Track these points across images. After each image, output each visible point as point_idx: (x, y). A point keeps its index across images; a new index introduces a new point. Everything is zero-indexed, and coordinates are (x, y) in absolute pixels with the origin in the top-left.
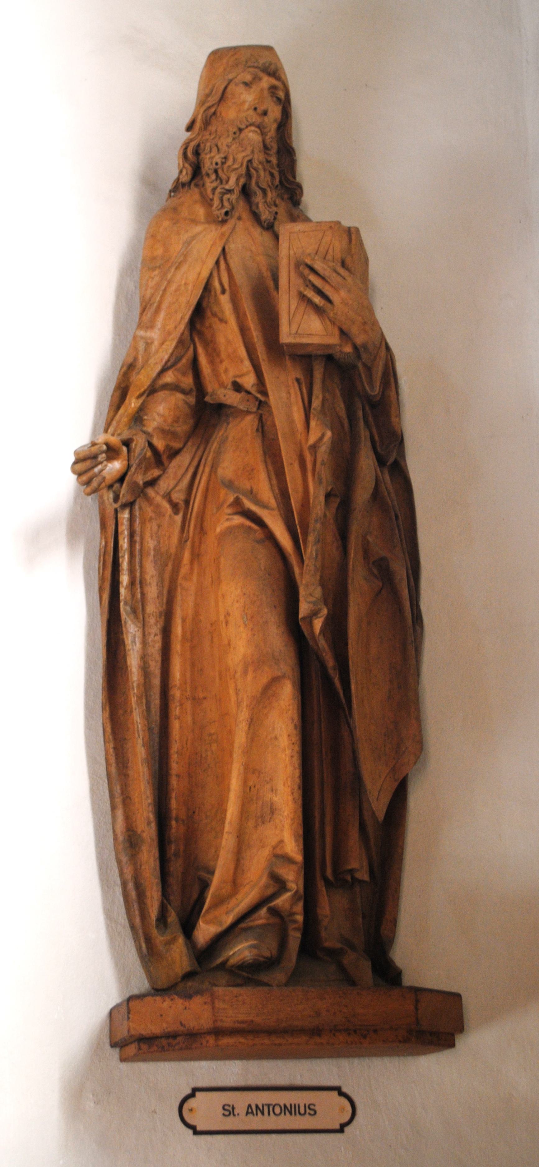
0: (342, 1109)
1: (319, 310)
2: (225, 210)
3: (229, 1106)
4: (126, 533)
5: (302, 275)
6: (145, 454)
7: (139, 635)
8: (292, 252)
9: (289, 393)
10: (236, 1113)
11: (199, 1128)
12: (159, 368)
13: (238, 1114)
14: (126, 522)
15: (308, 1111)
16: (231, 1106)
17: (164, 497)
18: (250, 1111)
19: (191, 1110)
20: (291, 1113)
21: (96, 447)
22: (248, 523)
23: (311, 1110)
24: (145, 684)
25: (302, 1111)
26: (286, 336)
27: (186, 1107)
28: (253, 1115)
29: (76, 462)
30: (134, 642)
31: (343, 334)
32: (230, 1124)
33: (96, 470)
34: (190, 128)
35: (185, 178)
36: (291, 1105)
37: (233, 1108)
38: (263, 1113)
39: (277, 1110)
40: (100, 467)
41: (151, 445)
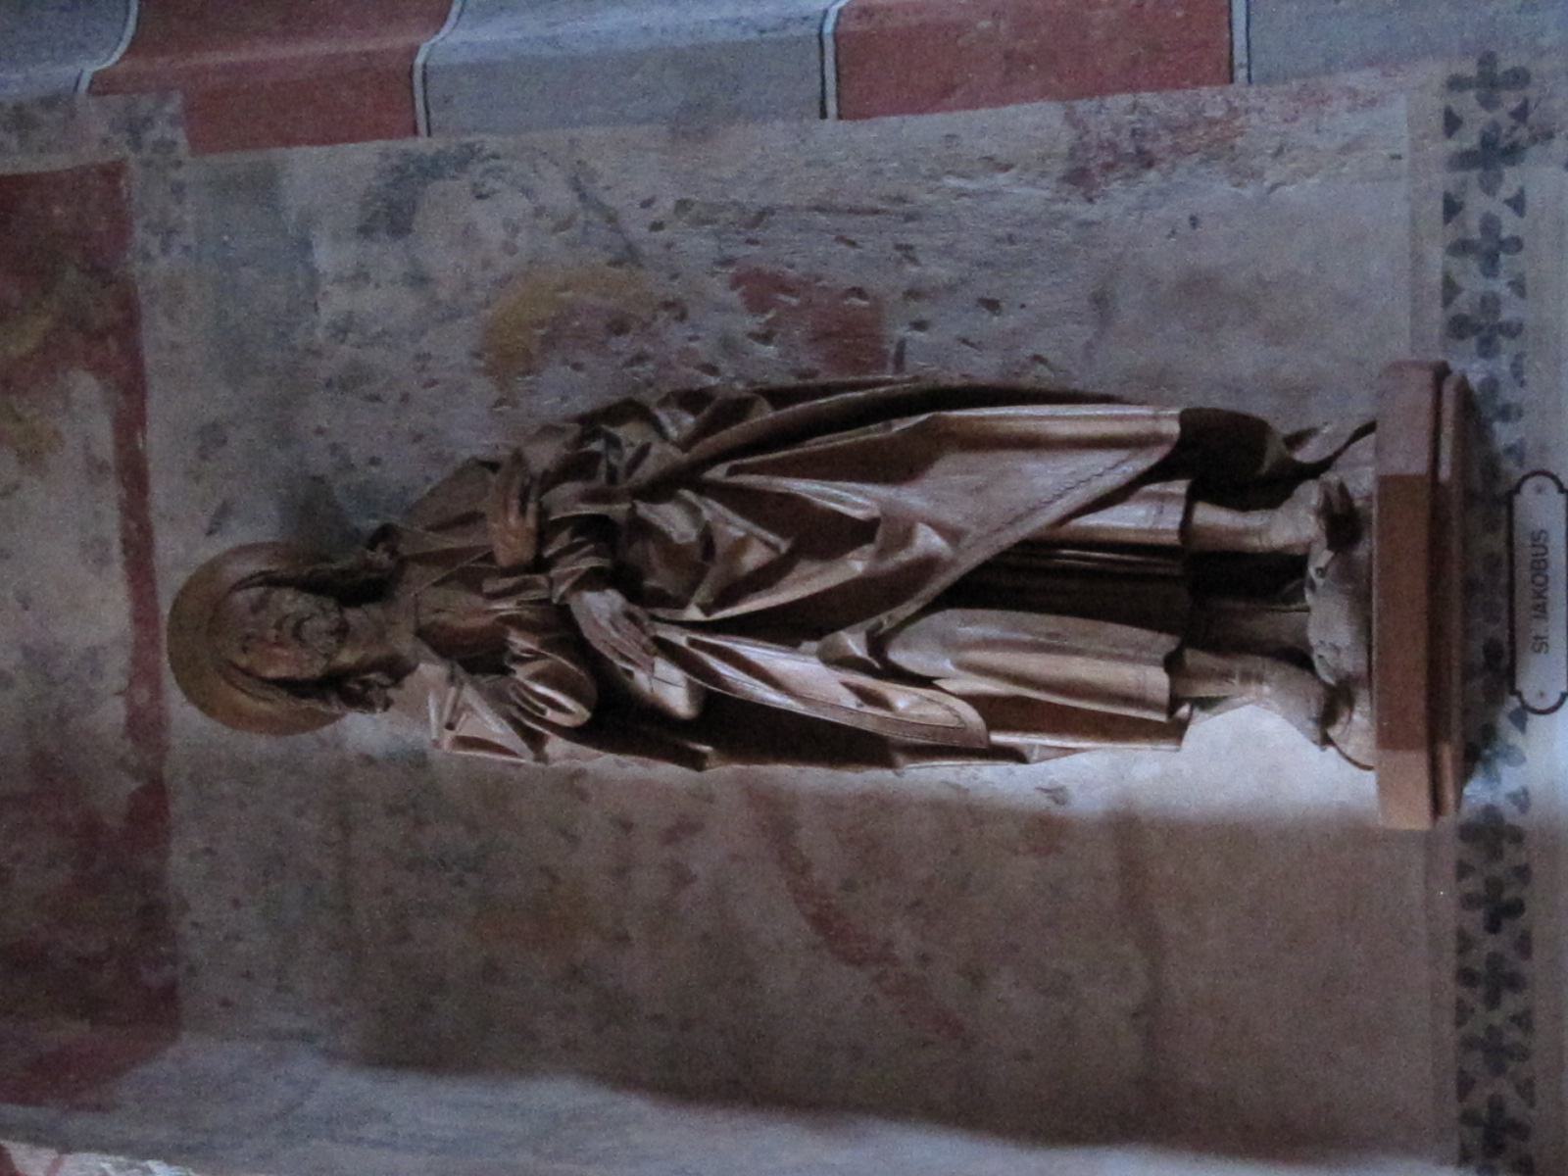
39: (1540, 579)
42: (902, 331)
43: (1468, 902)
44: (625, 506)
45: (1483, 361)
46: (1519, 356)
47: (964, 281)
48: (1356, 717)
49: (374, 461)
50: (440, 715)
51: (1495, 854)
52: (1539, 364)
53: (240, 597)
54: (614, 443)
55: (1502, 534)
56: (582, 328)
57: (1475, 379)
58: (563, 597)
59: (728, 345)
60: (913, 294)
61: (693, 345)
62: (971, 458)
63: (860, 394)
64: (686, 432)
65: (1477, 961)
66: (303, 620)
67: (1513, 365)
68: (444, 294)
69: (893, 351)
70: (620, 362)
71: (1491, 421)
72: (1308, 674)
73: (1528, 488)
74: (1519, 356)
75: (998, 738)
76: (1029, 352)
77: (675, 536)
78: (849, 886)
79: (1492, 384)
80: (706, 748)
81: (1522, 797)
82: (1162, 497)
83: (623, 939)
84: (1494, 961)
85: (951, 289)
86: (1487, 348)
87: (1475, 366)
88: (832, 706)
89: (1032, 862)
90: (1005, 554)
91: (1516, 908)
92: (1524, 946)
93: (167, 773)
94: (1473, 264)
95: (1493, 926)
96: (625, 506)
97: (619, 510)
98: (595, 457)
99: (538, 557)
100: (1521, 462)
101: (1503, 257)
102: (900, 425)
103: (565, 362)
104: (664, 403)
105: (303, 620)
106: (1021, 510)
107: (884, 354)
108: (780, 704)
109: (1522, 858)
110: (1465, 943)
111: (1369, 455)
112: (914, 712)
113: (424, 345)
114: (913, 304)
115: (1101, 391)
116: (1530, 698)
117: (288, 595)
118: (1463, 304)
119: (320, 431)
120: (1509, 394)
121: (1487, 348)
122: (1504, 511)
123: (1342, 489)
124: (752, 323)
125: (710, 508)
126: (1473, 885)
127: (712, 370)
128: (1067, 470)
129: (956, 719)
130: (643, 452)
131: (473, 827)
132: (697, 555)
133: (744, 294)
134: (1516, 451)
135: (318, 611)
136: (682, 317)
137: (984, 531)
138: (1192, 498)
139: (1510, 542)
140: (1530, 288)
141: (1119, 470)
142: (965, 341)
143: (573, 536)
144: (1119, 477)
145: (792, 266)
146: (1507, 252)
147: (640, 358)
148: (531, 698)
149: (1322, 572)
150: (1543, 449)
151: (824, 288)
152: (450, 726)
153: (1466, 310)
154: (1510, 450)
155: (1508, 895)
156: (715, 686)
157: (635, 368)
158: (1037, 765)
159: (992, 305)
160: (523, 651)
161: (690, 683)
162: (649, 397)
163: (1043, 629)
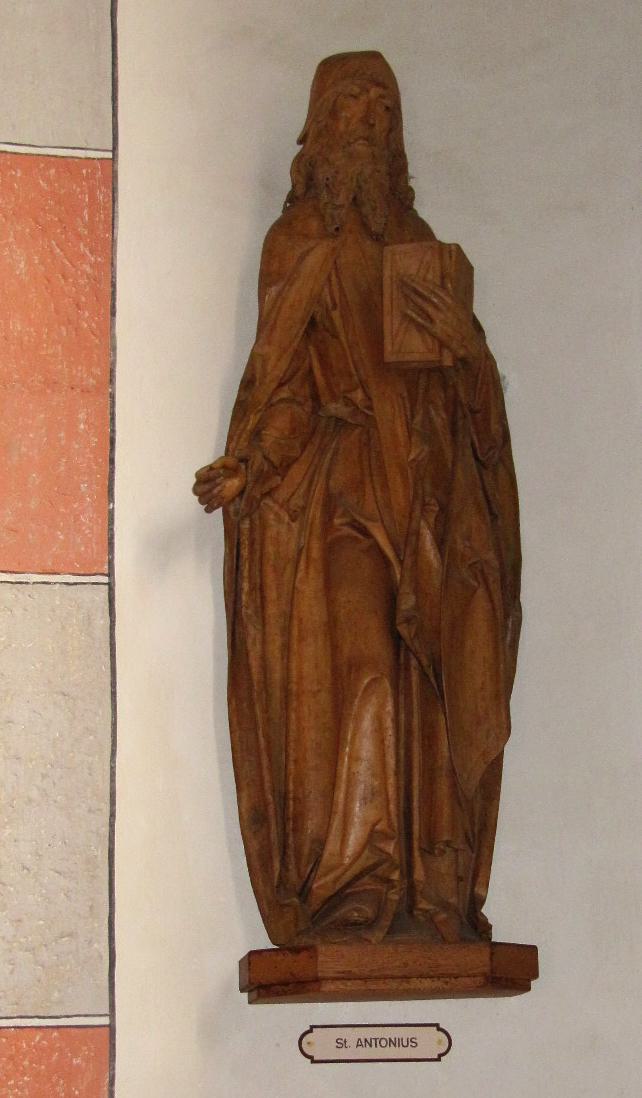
0: (440, 1042)
1: (420, 328)
2: (336, 226)
4: (247, 542)
5: (406, 297)
7: (259, 636)
8: (394, 274)
9: (393, 407)
11: (435, 1028)
12: (274, 385)
14: (246, 532)
17: (282, 506)
19: (309, 1043)
20: (395, 1045)
21: (213, 472)
22: (355, 533)
23: (412, 1042)
24: (265, 682)
25: (405, 1044)
26: (390, 356)
27: (304, 1046)
29: (196, 484)
30: (254, 644)
31: (442, 345)
32: (343, 1054)
33: (215, 491)
34: (301, 141)
35: (300, 191)
37: (345, 1042)
38: (371, 1046)
39: (383, 1043)
40: (219, 488)
41: (266, 458)
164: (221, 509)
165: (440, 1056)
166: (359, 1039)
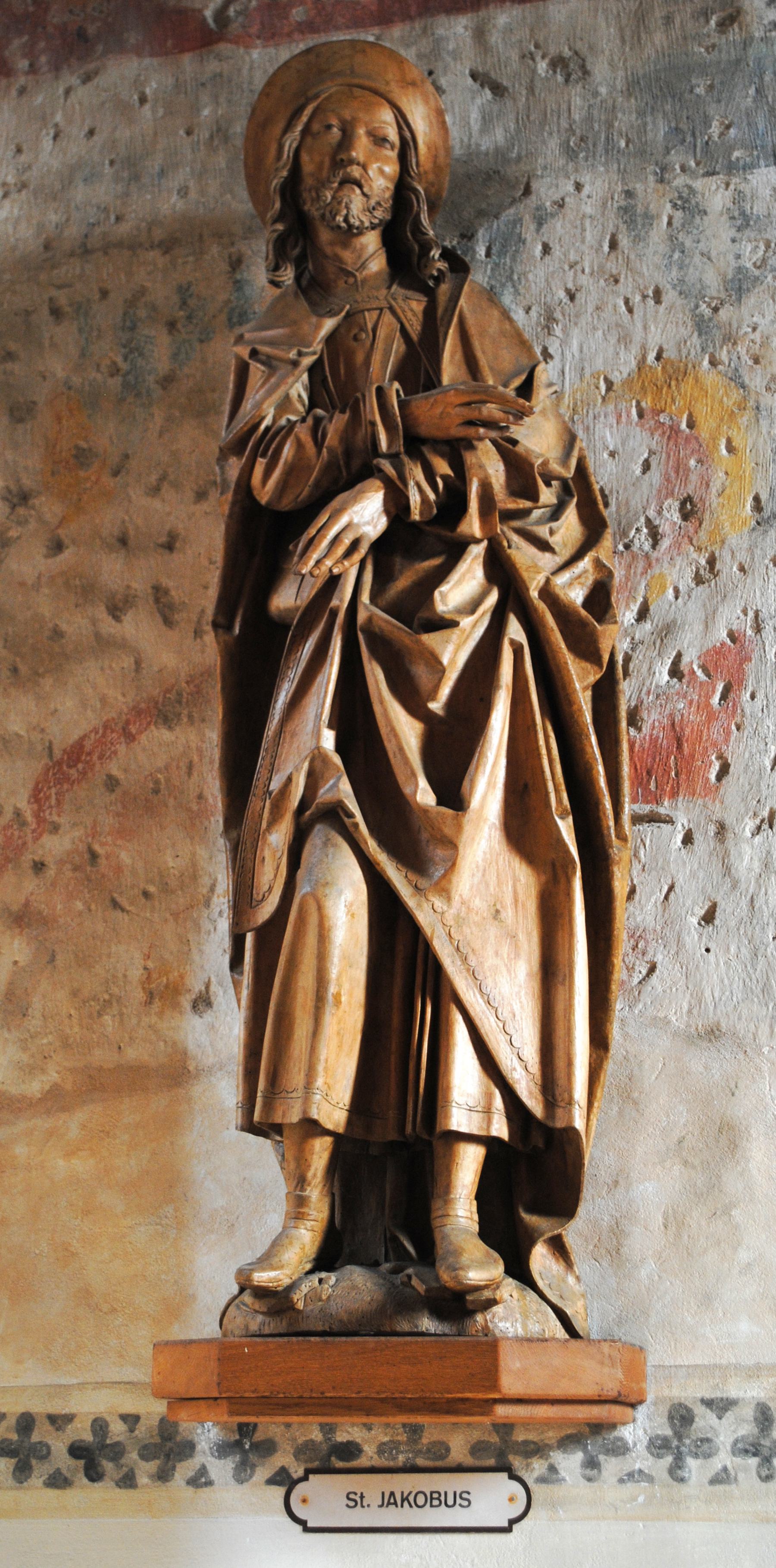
3: (356, 1494)
6: (175, 205)
10: (365, 1504)
11: (310, 1524)
13: (368, 1506)
15: (459, 1501)
16: (359, 1495)
18: (392, 1501)
28: (397, 1506)
36: (402, 1506)
37: (362, 1497)
39: (421, 1500)
42: (682, 821)
43: (100, 1426)
44: (477, 532)
45: (645, 1442)
46: (650, 1479)
47: (735, 885)
48: (260, 1318)
49: (546, 249)
50: (271, 343)
51: (146, 1454)
52: (641, 1499)
53: (387, 116)
54: (556, 513)
55: (469, 1461)
56: (688, 470)
57: (627, 1433)
58: (380, 470)
59: (667, 631)
60: (722, 829)
61: (671, 591)
62: (531, 906)
63: (602, 782)
64: (561, 593)
65: (41, 1434)
66: (360, 186)
67: (640, 1471)
68: (724, 314)
69: (662, 811)
70: (651, 513)
71: (585, 1450)
72: (308, 1266)
73: (516, 1488)
74: (650, 1479)
75: (249, 939)
76: (659, 958)
77: (444, 588)
78: (112, 783)
79: (620, 1449)
80: (237, 631)
81: (203, 1480)
82: (488, 1111)
83: (57, 547)
84: (43, 1453)
85: (727, 870)
86: (659, 1446)
87: (640, 1432)
88: (272, 764)
89: (136, 973)
90: (428, 947)
91: (94, 1474)
92: (58, 1481)
93: (224, 47)
94: (747, 1429)
95: (76, 1450)
96: (477, 532)
97: (472, 524)
98: (533, 496)
99: (424, 441)
100: (542, 1480)
101: (753, 1461)
102: (566, 828)
103: (651, 453)
104: (598, 564)
105: (360, 186)
106: (473, 961)
107: (658, 801)
108: (274, 708)
109: (143, 1480)
110: (58, 1421)
111: (535, 1329)
112: (267, 853)
113: (670, 296)
114: (712, 829)
115: (616, 1033)
116: (300, 1490)
117: (392, 169)
118: (705, 1420)
119: (578, 187)
120: (611, 1466)
121: (659, 1446)
122: (491, 1462)
123: (492, 1302)
124: (691, 659)
125: (475, 625)
126: (117, 1430)
127: (643, 614)
128: (517, 1008)
129: (260, 897)
130: (544, 546)
131: (167, 381)
132: (423, 614)
133: (723, 644)
134: (552, 1475)
135: (373, 202)
136: (699, 580)
137: (450, 921)
138: (490, 1142)
139: (460, 1469)
140: (720, 1488)
141: (516, 1063)
142: (671, 888)
143: (444, 478)
144: (509, 1063)
145: (753, 697)
146: (760, 1466)
147: (655, 536)
148: (278, 439)
149: (407, 1284)
150: (553, 1505)
151: (728, 733)
152: (254, 353)
153: (699, 1423)
154: (552, 1469)
155: (108, 1466)
156: (293, 636)
157: (645, 530)
158: (230, 979)
159: (709, 918)
160: (324, 429)
161: (297, 609)
162: (605, 549)
163: (346, 986)
164: (378, 312)
165: (512, 1522)
166: (392, 1494)
